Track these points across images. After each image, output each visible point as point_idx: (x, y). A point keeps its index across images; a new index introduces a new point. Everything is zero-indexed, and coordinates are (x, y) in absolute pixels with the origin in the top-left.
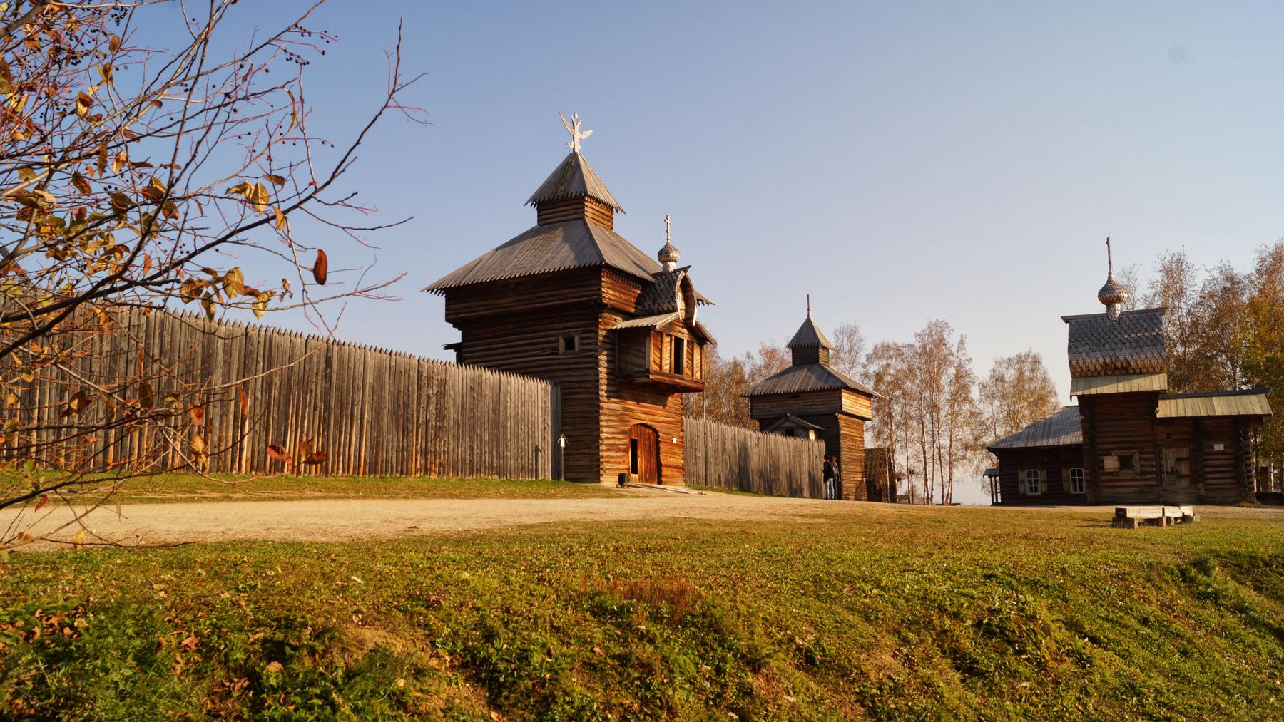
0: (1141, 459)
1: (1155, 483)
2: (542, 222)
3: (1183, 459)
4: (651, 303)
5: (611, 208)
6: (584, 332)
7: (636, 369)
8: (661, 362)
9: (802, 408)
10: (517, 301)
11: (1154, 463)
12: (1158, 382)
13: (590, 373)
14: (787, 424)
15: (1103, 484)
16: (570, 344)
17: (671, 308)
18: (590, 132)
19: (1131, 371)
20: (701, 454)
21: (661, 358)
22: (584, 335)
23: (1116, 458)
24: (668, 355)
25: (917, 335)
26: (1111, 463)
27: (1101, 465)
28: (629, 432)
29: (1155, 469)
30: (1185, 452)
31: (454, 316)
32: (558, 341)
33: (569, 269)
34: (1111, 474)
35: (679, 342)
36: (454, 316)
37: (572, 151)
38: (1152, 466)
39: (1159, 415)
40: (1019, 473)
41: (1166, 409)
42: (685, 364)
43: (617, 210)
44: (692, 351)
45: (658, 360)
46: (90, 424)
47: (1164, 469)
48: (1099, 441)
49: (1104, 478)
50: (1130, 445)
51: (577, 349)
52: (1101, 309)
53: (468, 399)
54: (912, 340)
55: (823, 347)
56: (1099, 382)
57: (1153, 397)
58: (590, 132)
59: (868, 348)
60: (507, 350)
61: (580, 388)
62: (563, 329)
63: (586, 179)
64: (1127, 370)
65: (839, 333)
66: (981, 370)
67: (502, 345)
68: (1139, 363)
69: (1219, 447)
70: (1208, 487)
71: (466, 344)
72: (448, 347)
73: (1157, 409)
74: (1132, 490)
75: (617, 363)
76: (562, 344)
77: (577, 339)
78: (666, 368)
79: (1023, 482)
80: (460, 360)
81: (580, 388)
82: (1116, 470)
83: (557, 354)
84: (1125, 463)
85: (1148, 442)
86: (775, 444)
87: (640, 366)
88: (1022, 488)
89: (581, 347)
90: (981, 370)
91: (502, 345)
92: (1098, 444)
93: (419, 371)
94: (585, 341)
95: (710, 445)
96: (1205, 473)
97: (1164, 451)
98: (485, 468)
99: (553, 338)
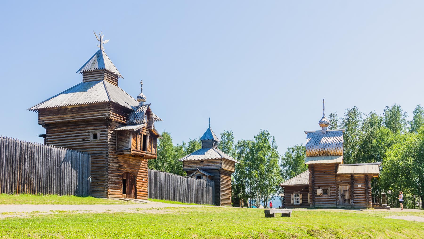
0: (331, 190)
1: (335, 200)
2: (85, 81)
3: (346, 190)
4: (133, 119)
5: (117, 76)
6: (102, 131)
7: (125, 148)
8: (136, 145)
9: (205, 166)
10: (71, 116)
11: (335, 192)
12: (340, 160)
13: (104, 150)
14: (198, 174)
15: (316, 200)
16: (95, 136)
17: (141, 122)
18: (109, 40)
19: (329, 155)
20: (157, 186)
21: (136, 144)
22: (101, 133)
23: (321, 189)
24: (140, 142)
25: (256, 138)
26: (319, 192)
27: (315, 192)
28: (122, 176)
29: (336, 194)
30: (347, 187)
31: (42, 122)
32: (90, 135)
33: (59, 106)
34: (319, 196)
35: (145, 137)
36: (42, 122)
37: (99, 49)
38: (334, 193)
39: (338, 173)
40: (292, 195)
41: (343, 170)
42: (148, 147)
43: (120, 77)
44: (151, 141)
45: (135, 145)
46: (182, 153)
47: (339, 194)
48: (315, 182)
49: (316, 197)
50: (327, 184)
51: (98, 139)
52: (320, 129)
53: (45, 160)
54: (252, 139)
55: (215, 141)
56: (317, 159)
57: (336, 166)
58: (109, 40)
59: (236, 142)
60: (67, 138)
61: (99, 156)
62: (92, 129)
63: (105, 64)
64: (328, 154)
65: (223, 135)
66: (282, 152)
67: (64, 136)
68: (332, 151)
69: (360, 186)
70: (355, 202)
71: (48, 135)
72: (40, 136)
73: (338, 170)
74: (327, 202)
75: (117, 145)
76: (91, 136)
77: (98, 134)
78: (139, 149)
79: (293, 199)
80: (46, 142)
81: (99, 156)
82: (321, 194)
83: (90, 141)
84: (325, 192)
85: (334, 183)
86: (192, 182)
87: (127, 147)
88: (292, 202)
89: (100, 138)
90: (282, 152)
91: (64, 136)
92: (315, 184)
93: (20, 147)
94: (102, 135)
95: (161, 182)
96: (354, 196)
97: (339, 186)
98: (53, 191)
99: (87, 134)
